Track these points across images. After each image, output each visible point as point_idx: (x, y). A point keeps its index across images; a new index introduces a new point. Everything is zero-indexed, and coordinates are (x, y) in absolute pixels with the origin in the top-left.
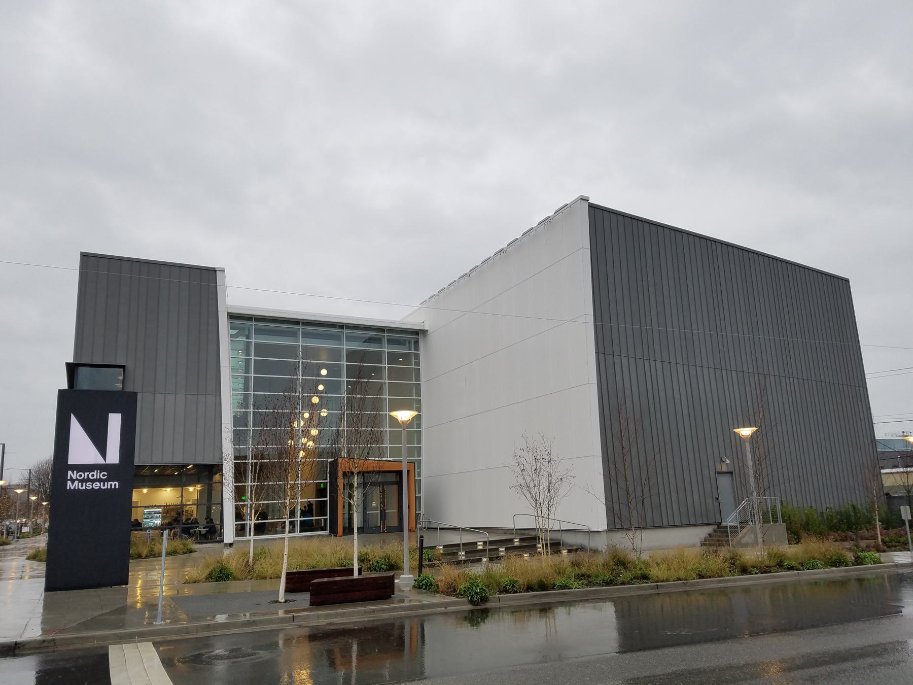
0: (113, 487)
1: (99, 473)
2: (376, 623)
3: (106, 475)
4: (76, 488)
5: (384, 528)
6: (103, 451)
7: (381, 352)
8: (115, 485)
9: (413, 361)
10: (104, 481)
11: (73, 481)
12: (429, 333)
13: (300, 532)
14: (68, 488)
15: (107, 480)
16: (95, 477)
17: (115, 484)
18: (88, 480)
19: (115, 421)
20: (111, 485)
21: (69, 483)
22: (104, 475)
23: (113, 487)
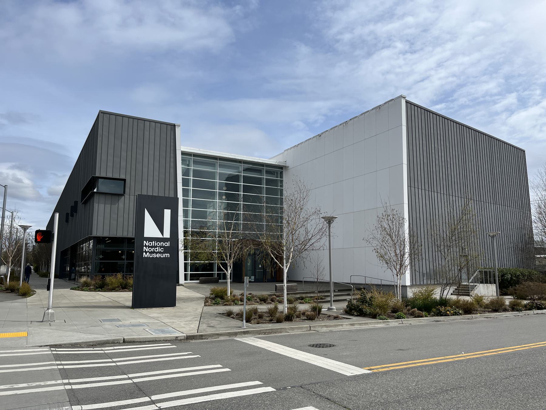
0: (167, 257)
2: (11, 301)
3: (163, 250)
4: (148, 257)
5: (265, 279)
6: (162, 231)
7: (214, 172)
8: (168, 255)
9: (279, 184)
10: (162, 253)
11: (146, 252)
12: (289, 168)
13: (190, 280)
14: (144, 257)
16: (157, 251)
17: (168, 255)
18: (154, 252)
19: (167, 213)
20: (166, 255)
21: (144, 253)
22: (162, 250)
23: (167, 257)
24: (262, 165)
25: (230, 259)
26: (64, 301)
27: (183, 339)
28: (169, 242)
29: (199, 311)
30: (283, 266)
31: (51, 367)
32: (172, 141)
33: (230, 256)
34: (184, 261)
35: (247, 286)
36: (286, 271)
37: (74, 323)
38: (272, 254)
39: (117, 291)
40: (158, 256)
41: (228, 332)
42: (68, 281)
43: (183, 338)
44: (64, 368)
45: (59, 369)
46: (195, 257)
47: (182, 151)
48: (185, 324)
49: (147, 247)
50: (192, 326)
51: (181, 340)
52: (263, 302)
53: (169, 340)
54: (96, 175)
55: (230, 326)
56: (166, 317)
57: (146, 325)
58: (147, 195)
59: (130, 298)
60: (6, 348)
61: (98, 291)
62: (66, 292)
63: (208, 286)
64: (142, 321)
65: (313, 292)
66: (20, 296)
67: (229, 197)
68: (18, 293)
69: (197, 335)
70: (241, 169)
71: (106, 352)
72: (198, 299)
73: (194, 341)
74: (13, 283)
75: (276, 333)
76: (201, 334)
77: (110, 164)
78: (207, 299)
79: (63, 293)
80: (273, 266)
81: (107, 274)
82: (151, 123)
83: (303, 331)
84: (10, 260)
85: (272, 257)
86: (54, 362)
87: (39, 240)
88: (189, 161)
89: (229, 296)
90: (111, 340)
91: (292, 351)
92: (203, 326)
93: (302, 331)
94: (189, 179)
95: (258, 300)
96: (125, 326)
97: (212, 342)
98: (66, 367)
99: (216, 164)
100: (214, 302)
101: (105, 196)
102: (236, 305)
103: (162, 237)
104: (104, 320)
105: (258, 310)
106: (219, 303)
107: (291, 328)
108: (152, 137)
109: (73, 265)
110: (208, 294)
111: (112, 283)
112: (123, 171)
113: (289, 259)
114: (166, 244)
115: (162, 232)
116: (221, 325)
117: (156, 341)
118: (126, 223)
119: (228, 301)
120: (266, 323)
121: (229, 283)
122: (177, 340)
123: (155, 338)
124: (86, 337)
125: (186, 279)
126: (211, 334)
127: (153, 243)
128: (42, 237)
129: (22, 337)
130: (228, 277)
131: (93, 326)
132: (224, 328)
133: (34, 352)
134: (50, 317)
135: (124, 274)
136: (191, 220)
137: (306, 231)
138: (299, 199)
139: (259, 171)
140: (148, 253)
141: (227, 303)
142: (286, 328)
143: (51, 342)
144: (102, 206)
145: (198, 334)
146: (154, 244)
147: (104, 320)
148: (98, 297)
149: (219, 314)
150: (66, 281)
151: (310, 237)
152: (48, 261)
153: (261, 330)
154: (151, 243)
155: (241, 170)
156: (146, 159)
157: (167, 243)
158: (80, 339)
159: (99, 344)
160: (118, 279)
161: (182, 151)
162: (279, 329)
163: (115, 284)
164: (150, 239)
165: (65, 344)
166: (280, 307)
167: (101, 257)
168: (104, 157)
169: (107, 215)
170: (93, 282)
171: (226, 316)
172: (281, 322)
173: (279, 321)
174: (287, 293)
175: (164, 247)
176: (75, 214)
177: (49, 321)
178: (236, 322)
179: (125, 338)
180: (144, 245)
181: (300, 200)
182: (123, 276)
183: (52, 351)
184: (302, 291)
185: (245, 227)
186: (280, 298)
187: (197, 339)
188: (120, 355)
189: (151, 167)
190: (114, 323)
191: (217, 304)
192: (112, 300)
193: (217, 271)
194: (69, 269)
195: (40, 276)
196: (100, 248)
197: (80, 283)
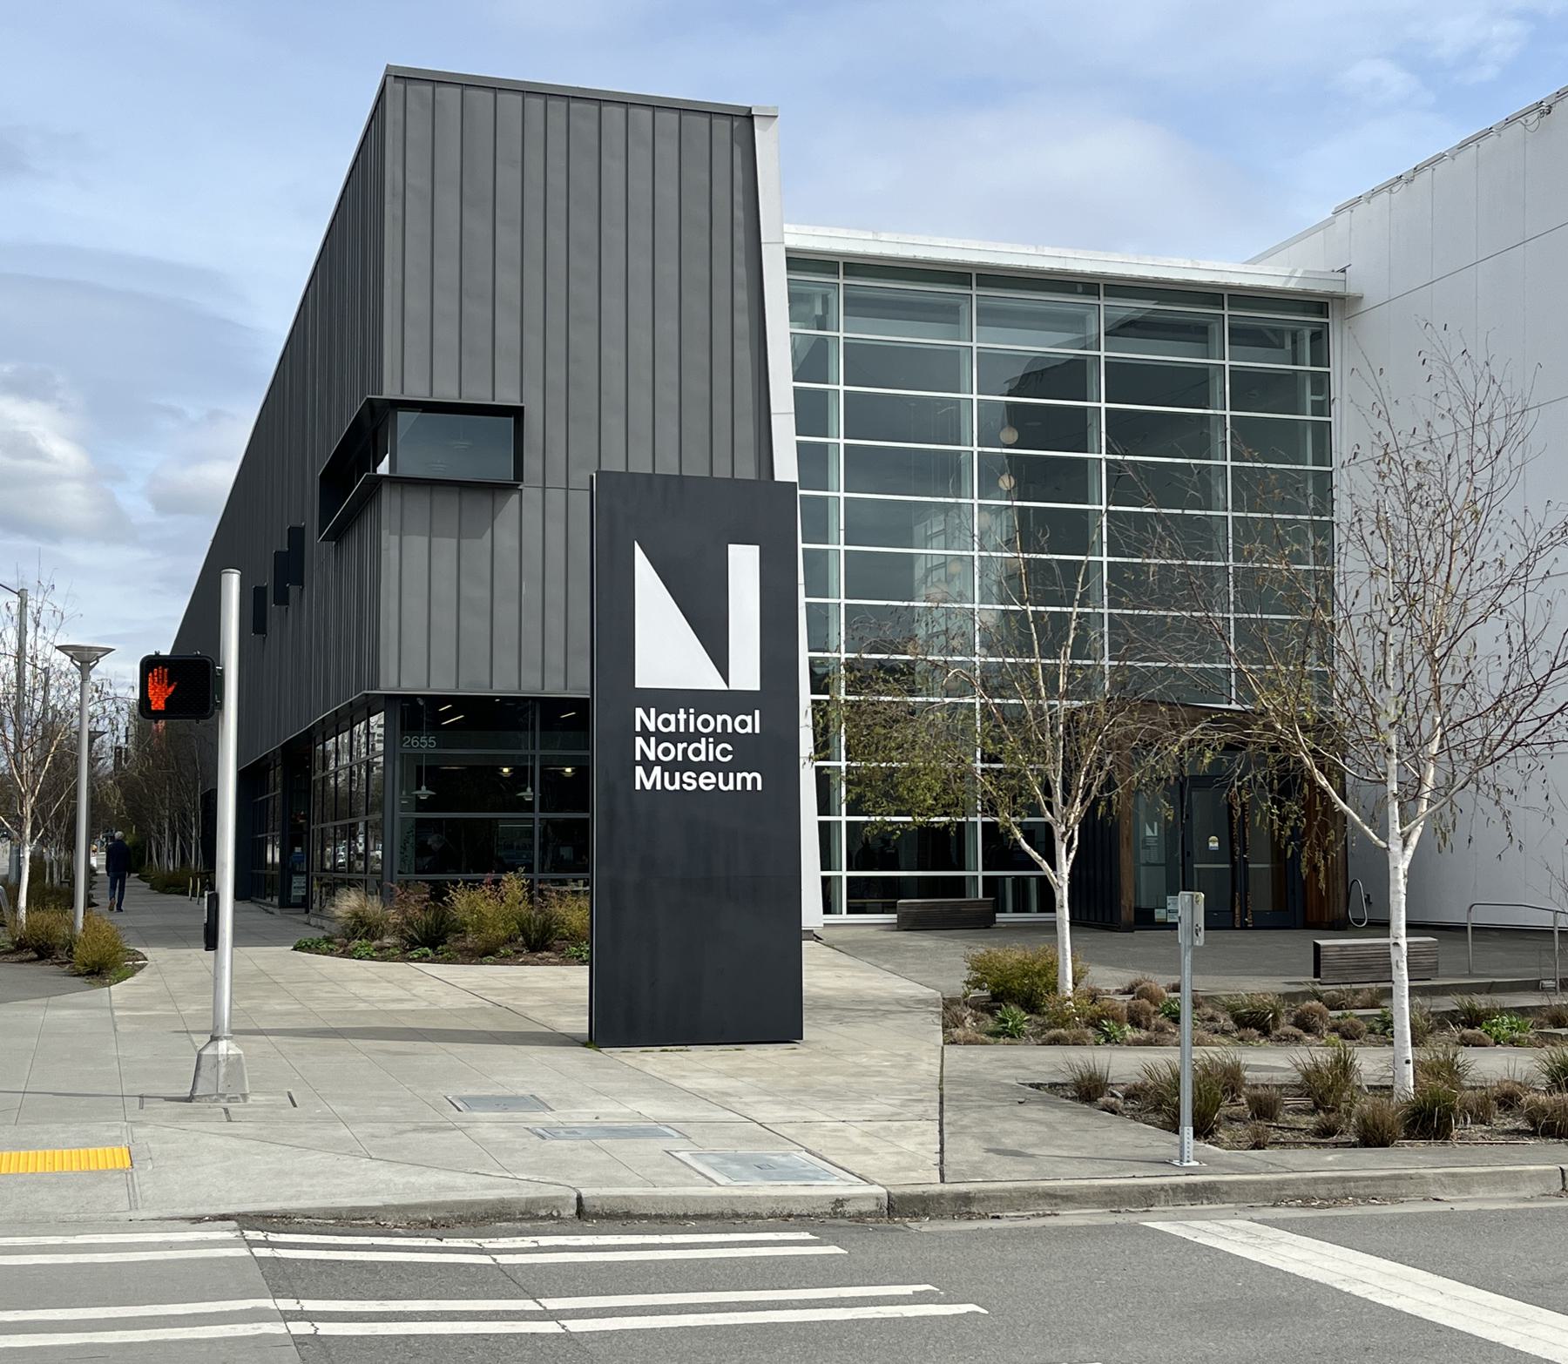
0: (749, 787)
1: (711, 746)
2: (44, 1001)
4: (659, 787)
5: (1244, 914)
6: (719, 656)
8: (754, 779)
9: (1309, 398)
10: (725, 769)
11: (648, 766)
12: (1364, 306)
13: (848, 912)
14: (638, 787)
15: (734, 767)
16: (702, 757)
18: (685, 765)
19: (744, 563)
20: (744, 779)
21: (639, 771)
22: (724, 753)
23: (749, 787)
24: (1212, 295)
25: (1065, 802)
26: (275, 1005)
27: (870, 1214)
28: (757, 713)
29: (924, 1066)
30: (1384, 836)
31: (256, 1325)
32: (739, 197)
33: (1067, 788)
34: (819, 814)
35: (1197, 943)
36: (1401, 863)
37: (333, 1107)
38: (1321, 769)
39: (505, 960)
40: (707, 785)
41: (1102, 1187)
42: (277, 911)
43: (870, 1206)
44: (319, 1333)
45: (293, 1336)
46: (886, 794)
47: (788, 250)
48: (866, 1134)
49: (653, 740)
50: (909, 1145)
51: (860, 1217)
52: (1256, 1032)
53: (799, 1216)
54: (385, 391)
55: (1108, 1155)
56: (768, 1093)
57: (676, 1135)
58: (627, 473)
59: (579, 997)
60: (39, 1221)
61: (419, 960)
62: (278, 959)
63: (941, 944)
64: (650, 1109)
65: (1535, 987)
66: (79, 975)
67: (1030, 478)
68: (70, 962)
69: (941, 1196)
70: (1098, 326)
71: (503, 1259)
72: (906, 1006)
73: (927, 1226)
74: (48, 917)
75: (1366, 1199)
76: (963, 1188)
77: (446, 333)
78: (956, 1009)
79: (263, 967)
80: (1318, 838)
81: (459, 877)
82: (632, 111)
83: (1522, 1194)
84: (27, 810)
85: (1320, 787)
86: (268, 1303)
87: (158, 704)
88: (825, 301)
89: (1069, 994)
90: (519, 1200)
91: (1499, 1307)
92: (965, 1151)
93: (1514, 1194)
94: (825, 392)
95: (1225, 1021)
96: (572, 1133)
97: (1027, 1235)
98: (325, 1329)
99: (964, 307)
100: (990, 1023)
101: (431, 495)
102: (1108, 1041)
103: (722, 686)
104: (473, 1102)
105: (1246, 1074)
106: (1021, 1032)
107: (1453, 1175)
108: (641, 186)
109: (294, 837)
110: (956, 981)
111: (479, 919)
112: (507, 367)
113: (1417, 798)
114: (743, 724)
115: (721, 661)
116: (1060, 1147)
117: (737, 1216)
118: (532, 627)
119: (1068, 1020)
120: (1298, 1145)
121: (1067, 925)
122: (843, 1216)
123: (731, 1199)
124: (400, 1180)
125: (828, 908)
126: (1016, 1189)
127: (677, 721)
128: (171, 689)
129: (107, 1171)
130: (1058, 897)
131: (424, 1129)
132: (1075, 1162)
133: (171, 1246)
134: (227, 1075)
135: (532, 880)
136: (843, 606)
137: (1510, 642)
138: (1464, 457)
139: (1196, 333)
140: (657, 770)
141: (1062, 1031)
142: (1422, 1177)
143: (241, 1201)
144: (417, 544)
145: (946, 1188)
146: (687, 721)
147: (473, 1102)
148: (421, 988)
149: (1031, 1085)
150: (270, 909)
151: (1539, 672)
152: (184, 815)
153: (1282, 1184)
154: (672, 718)
155: (1094, 331)
156: (613, 303)
157: (749, 719)
158: (375, 1193)
159: (461, 1220)
160: (509, 901)
161: (788, 250)
162: (1385, 1182)
163: (494, 927)
164: (666, 700)
165: (311, 1214)
166: (1369, 1063)
167: (424, 793)
168: (416, 303)
169: (444, 588)
170: (394, 916)
171: (1073, 1098)
172: (1384, 1143)
173: (1373, 1137)
174: (1410, 987)
175: (733, 738)
176: (293, 590)
177: (223, 1096)
178: (1133, 1135)
179: (585, 1192)
180: (638, 728)
181: (1470, 463)
182: (531, 888)
183: (252, 1244)
184: (1464, 976)
185: (1125, 637)
186: (1344, 1015)
187: (940, 1216)
188: (574, 1279)
189: (640, 337)
190: (518, 1115)
191: (1006, 1033)
192: (489, 1005)
193: (984, 870)
194: (277, 859)
195: (152, 888)
196: (418, 751)
197: (332, 919)
